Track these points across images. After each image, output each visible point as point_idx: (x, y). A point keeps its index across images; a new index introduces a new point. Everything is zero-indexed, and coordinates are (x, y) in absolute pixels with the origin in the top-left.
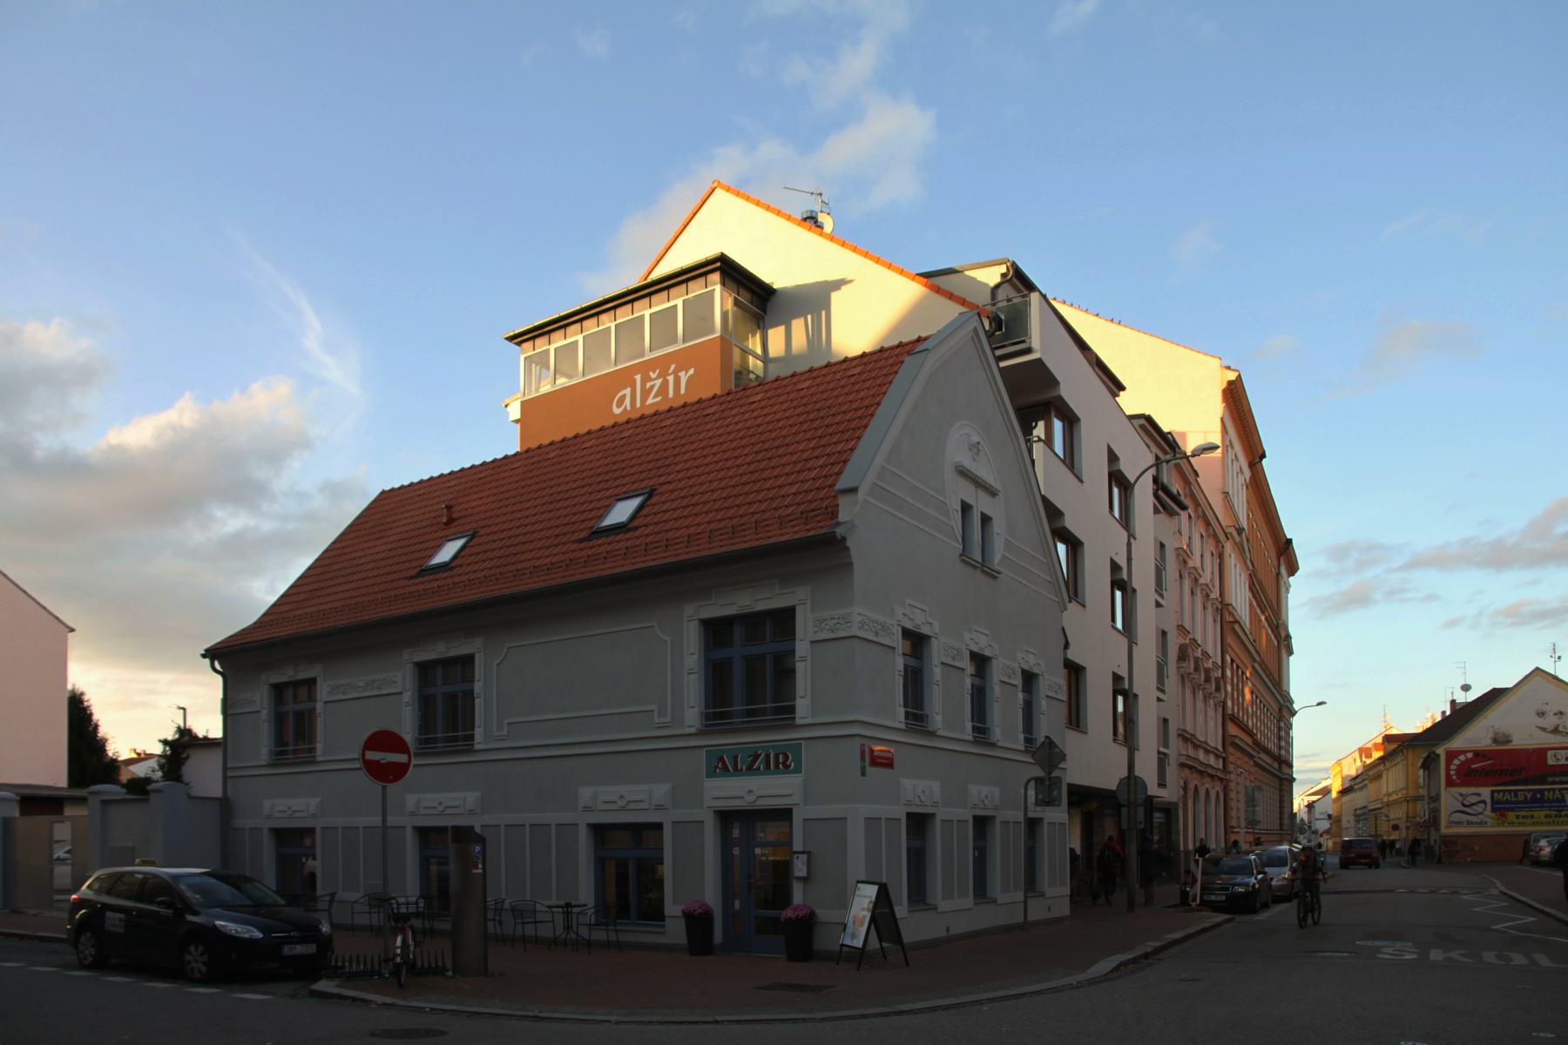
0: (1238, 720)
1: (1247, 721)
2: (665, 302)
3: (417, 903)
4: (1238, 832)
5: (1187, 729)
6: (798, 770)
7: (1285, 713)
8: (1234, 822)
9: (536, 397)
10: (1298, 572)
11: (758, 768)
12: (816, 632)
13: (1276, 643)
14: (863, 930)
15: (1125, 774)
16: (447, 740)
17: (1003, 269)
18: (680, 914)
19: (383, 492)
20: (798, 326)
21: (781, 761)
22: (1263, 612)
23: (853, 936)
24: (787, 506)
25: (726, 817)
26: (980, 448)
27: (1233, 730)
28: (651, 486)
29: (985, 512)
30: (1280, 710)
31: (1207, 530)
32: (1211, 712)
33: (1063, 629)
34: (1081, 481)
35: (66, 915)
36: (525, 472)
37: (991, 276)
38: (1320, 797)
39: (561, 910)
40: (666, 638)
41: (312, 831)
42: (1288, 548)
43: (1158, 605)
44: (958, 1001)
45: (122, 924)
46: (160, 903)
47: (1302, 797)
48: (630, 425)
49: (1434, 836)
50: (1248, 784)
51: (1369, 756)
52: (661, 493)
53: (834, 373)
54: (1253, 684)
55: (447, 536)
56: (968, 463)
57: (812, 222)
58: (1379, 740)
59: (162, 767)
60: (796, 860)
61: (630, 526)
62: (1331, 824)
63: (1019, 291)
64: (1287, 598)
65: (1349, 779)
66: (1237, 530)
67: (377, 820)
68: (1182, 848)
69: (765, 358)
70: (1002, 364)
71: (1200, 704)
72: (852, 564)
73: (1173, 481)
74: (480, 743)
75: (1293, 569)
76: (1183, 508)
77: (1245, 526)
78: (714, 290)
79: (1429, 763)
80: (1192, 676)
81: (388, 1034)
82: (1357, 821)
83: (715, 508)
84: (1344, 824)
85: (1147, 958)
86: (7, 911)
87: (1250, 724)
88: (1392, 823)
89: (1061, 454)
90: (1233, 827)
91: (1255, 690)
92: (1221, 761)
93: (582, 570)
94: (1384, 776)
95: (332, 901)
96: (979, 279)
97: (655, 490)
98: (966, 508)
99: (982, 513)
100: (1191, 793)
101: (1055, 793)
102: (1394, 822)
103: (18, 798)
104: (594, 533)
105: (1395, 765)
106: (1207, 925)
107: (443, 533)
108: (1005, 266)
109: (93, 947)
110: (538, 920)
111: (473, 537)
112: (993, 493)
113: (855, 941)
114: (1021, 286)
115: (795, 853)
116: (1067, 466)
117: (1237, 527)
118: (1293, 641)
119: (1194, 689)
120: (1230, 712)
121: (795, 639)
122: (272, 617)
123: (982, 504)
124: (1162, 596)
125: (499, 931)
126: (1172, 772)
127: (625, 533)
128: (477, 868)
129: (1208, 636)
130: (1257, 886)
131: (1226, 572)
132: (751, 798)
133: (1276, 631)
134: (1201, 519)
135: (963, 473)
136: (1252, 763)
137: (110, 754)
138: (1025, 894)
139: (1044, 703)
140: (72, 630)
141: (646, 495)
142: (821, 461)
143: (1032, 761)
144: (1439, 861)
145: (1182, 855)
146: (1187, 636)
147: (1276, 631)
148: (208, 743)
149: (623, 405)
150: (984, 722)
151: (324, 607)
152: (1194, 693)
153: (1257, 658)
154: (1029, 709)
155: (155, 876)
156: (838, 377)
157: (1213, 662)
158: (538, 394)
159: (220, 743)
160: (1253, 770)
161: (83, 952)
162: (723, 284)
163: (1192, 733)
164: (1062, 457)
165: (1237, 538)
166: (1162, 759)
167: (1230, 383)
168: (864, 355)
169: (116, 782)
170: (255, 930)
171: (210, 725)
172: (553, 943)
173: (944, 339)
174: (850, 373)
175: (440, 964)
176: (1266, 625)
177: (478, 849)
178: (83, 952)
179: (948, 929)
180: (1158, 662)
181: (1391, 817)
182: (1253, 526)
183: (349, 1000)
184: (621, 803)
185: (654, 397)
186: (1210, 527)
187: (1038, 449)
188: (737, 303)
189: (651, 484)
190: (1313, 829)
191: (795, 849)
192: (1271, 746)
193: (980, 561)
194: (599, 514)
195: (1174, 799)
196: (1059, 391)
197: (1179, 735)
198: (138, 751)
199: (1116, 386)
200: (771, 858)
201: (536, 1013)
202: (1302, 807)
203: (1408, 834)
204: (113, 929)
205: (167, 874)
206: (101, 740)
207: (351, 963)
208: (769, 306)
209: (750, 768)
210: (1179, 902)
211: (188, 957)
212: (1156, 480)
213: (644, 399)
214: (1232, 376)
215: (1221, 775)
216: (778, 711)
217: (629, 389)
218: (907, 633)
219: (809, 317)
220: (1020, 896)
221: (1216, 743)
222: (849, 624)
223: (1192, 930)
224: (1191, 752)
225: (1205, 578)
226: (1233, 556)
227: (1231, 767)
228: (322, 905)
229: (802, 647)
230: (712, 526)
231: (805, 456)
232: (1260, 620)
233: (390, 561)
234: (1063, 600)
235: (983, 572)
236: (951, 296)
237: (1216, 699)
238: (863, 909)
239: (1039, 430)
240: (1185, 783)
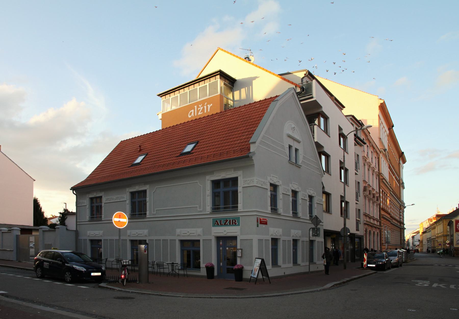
0: (385, 210)
1: (387, 209)
2: (203, 84)
3: (129, 262)
4: (385, 245)
5: (367, 213)
6: (239, 225)
7: (402, 207)
9: (166, 113)
10: (406, 162)
11: (227, 224)
12: (244, 184)
13: (399, 185)
14: (257, 272)
15: (343, 227)
16: (139, 214)
17: (305, 72)
18: (205, 267)
19: (122, 141)
20: (243, 90)
21: (234, 222)
22: (394, 175)
23: (254, 274)
24: (236, 147)
25: (219, 239)
26: (295, 128)
27: (383, 213)
29: (296, 148)
30: (400, 206)
31: (374, 150)
32: (375, 207)
33: (322, 182)
34: (330, 137)
35: (33, 263)
36: (162, 136)
37: (302, 75)
39: (171, 265)
40: (201, 186)
41: (101, 240)
42: (402, 155)
43: (356, 174)
44: (282, 294)
45: (48, 266)
46: (58, 260)
47: (411, 234)
48: (192, 122)
49: (452, 248)
51: (431, 221)
52: (201, 143)
53: (251, 106)
54: (390, 198)
55: (140, 155)
56: (291, 133)
57: (248, 59)
58: (435, 216)
59: (59, 220)
60: (238, 251)
61: (192, 152)
62: (419, 243)
64: (403, 171)
65: (425, 228)
66: (384, 150)
69: (233, 100)
70: (301, 102)
71: (371, 205)
72: (254, 164)
73: (362, 135)
74: (148, 216)
75: (404, 162)
76: (365, 144)
78: (218, 80)
79: (450, 224)
80: (368, 196)
81: (119, 298)
82: (428, 242)
83: (216, 147)
84: (424, 243)
85: (344, 283)
86: (17, 261)
87: (389, 211)
91: (391, 200)
92: (379, 223)
93: (177, 166)
94: (436, 228)
95: (106, 261)
96: (297, 76)
97: (199, 141)
98: (290, 147)
99: (296, 148)
100: (368, 233)
101: (318, 233)
103: (20, 229)
104: (181, 154)
106: (367, 274)
107: (138, 154)
108: (305, 71)
109: (40, 272)
110: (164, 267)
111: (147, 155)
112: (299, 142)
113: (255, 276)
114: (311, 78)
115: (238, 249)
116: (325, 133)
118: (405, 184)
119: (369, 200)
120: (382, 207)
121: (238, 186)
122: (90, 178)
123: (295, 145)
124: (357, 171)
125: (153, 271)
126: (361, 226)
129: (374, 184)
130: (385, 262)
131: (380, 163)
132: (225, 233)
134: (371, 147)
135: (289, 136)
136: (390, 223)
137: (45, 216)
138: (309, 263)
139: (316, 205)
140: (35, 180)
141: (196, 143)
142: (247, 133)
143: (311, 223)
144: (454, 256)
146: (366, 184)
148: (72, 214)
149: (192, 115)
150: (296, 211)
151: (104, 176)
153: (391, 190)
154: (311, 207)
155: (57, 252)
156: (252, 108)
157: (376, 192)
158: (167, 112)
159: (75, 214)
160: (390, 225)
161: (38, 273)
162: (221, 79)
163: (368, 214)
164: (323, 130)
165: (384, 153)
166: (358, 222)
167: (381, 104)
168: (260, 101)
169: (47, 225)
170: (84, 268)
171: (72, 208)
172: (169, 274)
173: (283, 96)
174: (256, 106)
175: (135, 279)
176: (395, 180)
178: (38, 273)
179: (284, 273)
181: (439, 241)
182: (390, 148)
183: (109, 289)
184: (188, 234)
185: (201, 112)
188: (225, 84)
189: (198, 140)
190: (414, 244)
191: (238, 248)
192: (397, 218)
193: (295, 163)
194: (183, 149)
195: (362, 234)
196: (322, 109)
197: (364, 215)
198: (53, 215)
199: (341, 106)
200: (233, 251)
201: (161, 294)
202: (410, 237)
203: (444, 247)
204: (45, 267)
205: (60, 252)
206: (43, 212)
207: (110, 278)
208: (235, 84)
209: (225, 224)
211: (66, 276)
212: (355, 135)
213: (197, 113)
214: (382, 102)
215: (379, 227)
216: (233, 207)
217: (193, 110)
218: (271, 185)
219: (246, 88)
220: (308, 263)
221: (377, 217)
222: (254, 182)
223: (361, 275)
224: (368, 220)
225: (373, 165)
226: (383, 158)
227: (382, 225)
228: (103, 262)
229: (240, 189)
230: (214, 153)
231: (242, 132)
232: (393, 178)
233: (123, 162)
234: (322, 174)
235: (296, 165)
236: (289, 81)
237: (377, 203)
238: (257, 266)
239: (316, 122)
240: (366, 229)
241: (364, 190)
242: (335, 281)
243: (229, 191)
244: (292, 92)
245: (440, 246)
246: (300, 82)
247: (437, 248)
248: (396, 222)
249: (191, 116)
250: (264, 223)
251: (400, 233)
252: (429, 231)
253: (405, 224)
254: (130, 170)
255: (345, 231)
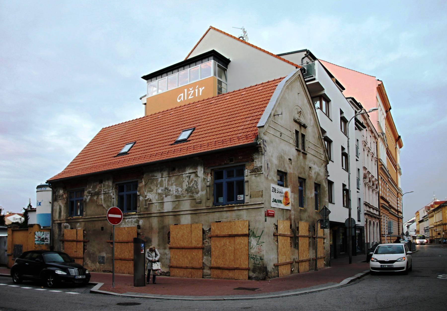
1: (385, 197)
4: (384, 236)
7: (399, 195)
8: (383, 233)
13: (396, 171)
15: (348, 217)
27: (382, 201)
28: (194, 127)
30: (398, 194)
32: (374, 195)
38: (411, 223)
42: (399, 139)
43: (357, 160)
50: (387, 219)
51: (429, 210)
52: (198, 129)
61: (188, 139)
63: (311, 60)
67: (289, 238)
68: (366, 242)
70: (307, 83)
76: (364, 127)
77: (385, 132)
82: (425, 232)
88: (438, 232)
89: (325, 112)
90: (383, 235)
94: (434, 216)
97: (196, 128)
98: (297, 132)
100: (368, 223)
102: (438, 232)
105: (438, 212)
117: (382, 133)
119: (369, 188)
120: (381, 195)
122: (68, 170)
126: (362, 216)
127: (186, 142)
128: (142, 251)
129: (373, 170)
133: (395, 167)
136: (388, 212)
141: (193, 130)
145: (366, 244)
147: (395, 167)
149: (181, 99)
152: (369, 189)
153: (390, 177)
160: (389, 215)
165: (382, 137)
177: (143, 245)
180: (357, 179)
185: (191, 96)
186: (370, 127)
187: (318, 111)
195: (363, 225)
197: (364, 204)
210: (366, 260)
214: (380, 83)
215: (378, 217)
224: (368, 209)
227: (381, 214)
239: (318, 104)
241: (364, 177)
242: (351, 277)
243: (234, 181)
244: (298, 74)
245: (438, 236)
246: (301, 63)
247: (435, 238)
248: (394, 211)
249: (180, 100)
250: (271, 215)
251: (397, 223)
252: (426, 219)
253: (330, 212)
254: (116, 160)
255: (350, 222)
